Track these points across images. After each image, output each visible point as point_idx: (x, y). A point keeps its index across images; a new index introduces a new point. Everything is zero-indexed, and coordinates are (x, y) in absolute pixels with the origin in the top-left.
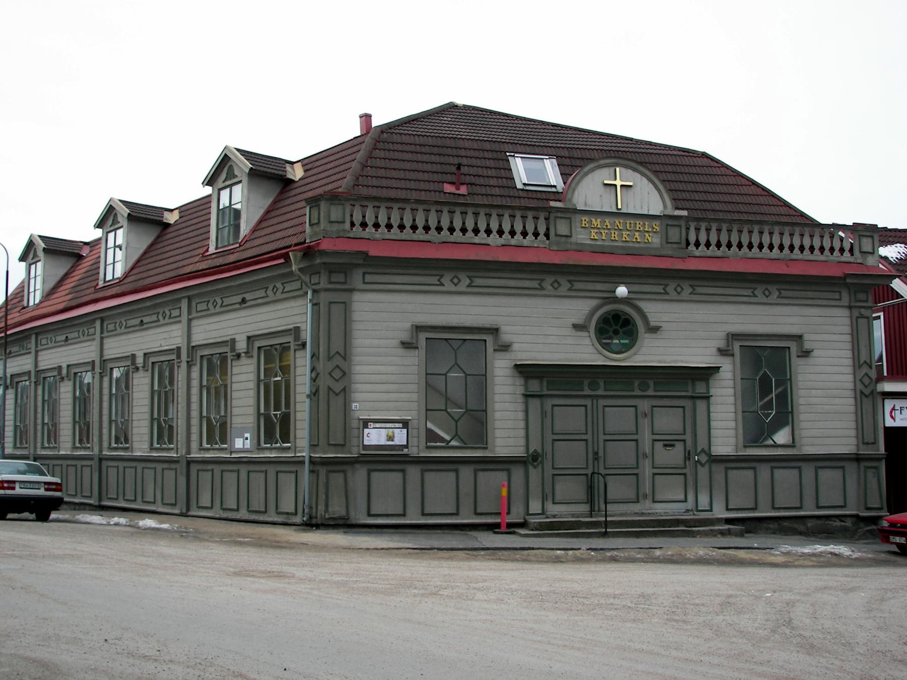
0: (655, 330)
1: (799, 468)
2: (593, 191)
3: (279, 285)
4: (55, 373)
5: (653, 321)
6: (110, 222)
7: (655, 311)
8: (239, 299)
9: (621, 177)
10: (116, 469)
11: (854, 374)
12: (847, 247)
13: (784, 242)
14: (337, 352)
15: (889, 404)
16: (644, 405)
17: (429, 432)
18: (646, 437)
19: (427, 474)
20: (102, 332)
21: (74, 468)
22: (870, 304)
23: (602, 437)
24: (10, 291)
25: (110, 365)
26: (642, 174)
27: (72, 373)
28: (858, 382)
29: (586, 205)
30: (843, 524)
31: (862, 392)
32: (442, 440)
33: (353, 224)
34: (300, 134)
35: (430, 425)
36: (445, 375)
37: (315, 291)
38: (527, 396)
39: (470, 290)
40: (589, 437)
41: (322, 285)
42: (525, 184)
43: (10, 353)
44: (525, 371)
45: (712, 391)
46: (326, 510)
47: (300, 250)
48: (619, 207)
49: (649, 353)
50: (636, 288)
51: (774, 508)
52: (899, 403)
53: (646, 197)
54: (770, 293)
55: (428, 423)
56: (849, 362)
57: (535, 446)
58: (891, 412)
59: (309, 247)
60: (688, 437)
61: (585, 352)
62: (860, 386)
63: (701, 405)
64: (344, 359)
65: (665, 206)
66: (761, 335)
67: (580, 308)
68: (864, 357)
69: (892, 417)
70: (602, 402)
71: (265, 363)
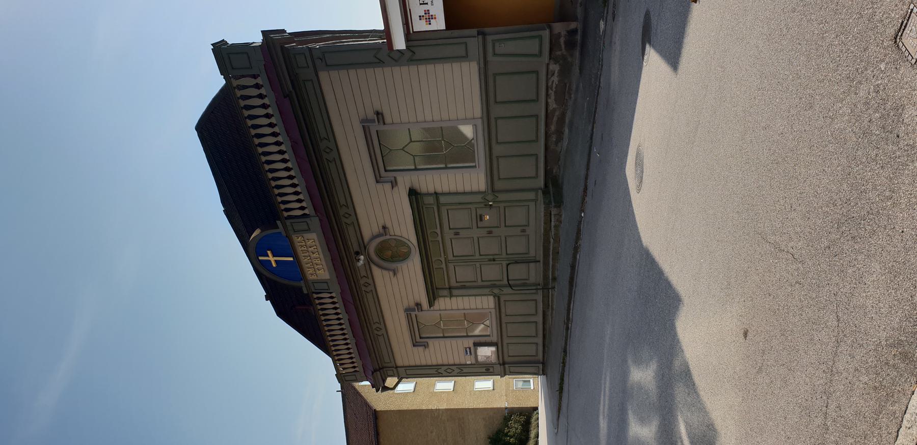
0: (384, 228)
34: (263, 293)
39: (370, 276)
45: (431, 190)
49: (404, 227)
51: (537, 140)
52: (416, 10)
56: (378, 71)
61: (413, 267)
63: (443, 199)
70: (450, 257)
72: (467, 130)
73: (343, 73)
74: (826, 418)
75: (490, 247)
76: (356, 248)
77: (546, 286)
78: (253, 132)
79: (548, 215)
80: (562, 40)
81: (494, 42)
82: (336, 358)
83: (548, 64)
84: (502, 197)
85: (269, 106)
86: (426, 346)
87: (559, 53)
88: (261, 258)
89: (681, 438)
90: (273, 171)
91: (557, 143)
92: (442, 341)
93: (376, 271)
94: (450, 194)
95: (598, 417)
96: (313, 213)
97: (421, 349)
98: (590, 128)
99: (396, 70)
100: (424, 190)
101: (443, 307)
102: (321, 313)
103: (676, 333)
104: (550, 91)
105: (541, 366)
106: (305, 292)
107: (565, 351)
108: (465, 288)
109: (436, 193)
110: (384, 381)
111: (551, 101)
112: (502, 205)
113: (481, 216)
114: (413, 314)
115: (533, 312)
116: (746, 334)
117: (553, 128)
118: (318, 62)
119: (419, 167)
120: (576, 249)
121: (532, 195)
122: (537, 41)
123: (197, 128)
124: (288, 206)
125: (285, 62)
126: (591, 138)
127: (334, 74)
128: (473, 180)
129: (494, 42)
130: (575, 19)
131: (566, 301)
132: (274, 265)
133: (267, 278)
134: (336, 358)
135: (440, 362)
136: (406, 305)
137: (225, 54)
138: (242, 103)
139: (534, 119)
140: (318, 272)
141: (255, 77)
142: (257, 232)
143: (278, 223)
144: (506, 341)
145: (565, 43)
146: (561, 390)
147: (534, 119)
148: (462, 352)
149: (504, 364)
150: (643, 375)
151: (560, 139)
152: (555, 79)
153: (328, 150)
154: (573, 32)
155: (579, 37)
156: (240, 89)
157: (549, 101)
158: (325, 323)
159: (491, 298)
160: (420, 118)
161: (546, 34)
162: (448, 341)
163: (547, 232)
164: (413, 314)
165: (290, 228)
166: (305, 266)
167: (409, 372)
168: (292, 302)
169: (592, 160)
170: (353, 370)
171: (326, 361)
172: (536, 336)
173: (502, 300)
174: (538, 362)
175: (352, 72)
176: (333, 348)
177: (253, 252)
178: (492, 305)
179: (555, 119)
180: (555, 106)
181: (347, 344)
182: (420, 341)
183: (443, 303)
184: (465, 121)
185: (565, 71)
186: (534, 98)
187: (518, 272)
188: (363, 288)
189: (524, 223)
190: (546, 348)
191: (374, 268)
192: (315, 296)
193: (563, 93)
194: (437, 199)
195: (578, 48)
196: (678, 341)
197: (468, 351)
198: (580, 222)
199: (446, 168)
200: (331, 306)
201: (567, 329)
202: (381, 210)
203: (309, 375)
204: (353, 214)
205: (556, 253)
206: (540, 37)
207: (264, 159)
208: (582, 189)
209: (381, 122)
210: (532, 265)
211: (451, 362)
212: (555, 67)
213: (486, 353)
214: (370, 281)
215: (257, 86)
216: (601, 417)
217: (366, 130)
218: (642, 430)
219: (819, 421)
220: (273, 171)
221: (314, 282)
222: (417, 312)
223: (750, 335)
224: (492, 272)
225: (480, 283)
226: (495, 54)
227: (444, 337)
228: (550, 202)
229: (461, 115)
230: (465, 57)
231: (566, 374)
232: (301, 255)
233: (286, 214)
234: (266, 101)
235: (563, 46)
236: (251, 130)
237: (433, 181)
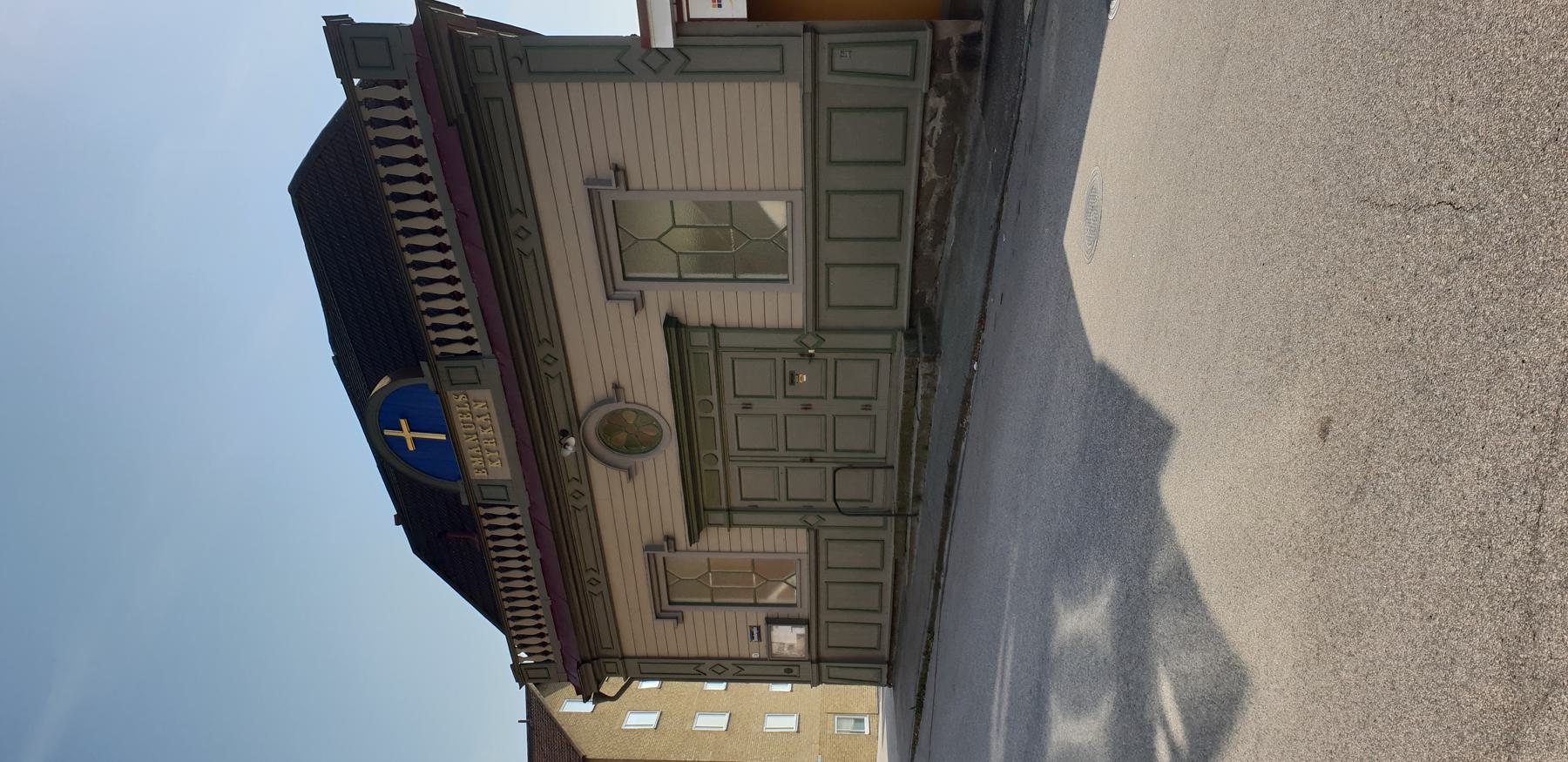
0: (616, 387)
1: (831, 110)
19: (865, 445)
30: (940, 115)
39: (584, 479)
40: (782, 467)
44: (697, 520)
45: (706, 321)
49: (653, 393)
51: (899, 237)
56: (623, 87)
63: (725, 339)
70: (733, 449)
72: (776, 212)
73: (559, 88)
74: (1535, 537)
75: (806, 435)
76: (564, 425)
77: (902, 513)
78: (410, 258)
79: (912, 375)
80: (953, 52)
81: (832, 47)
82: (514, 633)
83: (926, 96)
84: (832, 340)
85: (445, 231)
86: (679, 619)
87: (946, 76)
88: (387, 432)
89: (1161, 709)
90: (442, 342)
91: (934, 245)
92: (709, 612)
93: (596, 468)
94: (739, 329)
95: (988, 729)
96: (488, 351)
97: (670, 624)
98: (996, 203)
99: (655, 88)
100: (692, 320)
101: (714, 547)
102: (491, 544)
103: (1158, 498)
104: (927, 147)
105: (885, 668)
106: (465, 502)
107: (931, 631)
108: (756, 509)
109: (714, 326)
110: (599, 683)
111: (929, 165)
112: (831, 357)
113: (792, 375)
114: (660, 555)
115: (876, 606)
116: (1324, 431)
117: (929, 216)
118: (514, 65)
119: (686, 276)
120: (960, 433)
121: (883, 341)
122: (909, 49)
123: (291, 190)
124: (425, 273)
125: (454, 57)
126: (998, 221)
127: (542, 88)
128: (780, 305)
129: (832, 47)
130: (977, 15)
131: (937, 535)
132: (411, 447)
133: (397, 472)
134: (514, 633)
135: (703, 653)
136: (647, 539)
137: (344, 38)
138: (389, 189)
139: (900, 116)
140: (490, 465)
141: (398, 85)
142: (385, 381)
143: (424, 366)
144: (824, 617)
145: (958, 57)
146: (920, 706)
147: (900, 116)
148: (744, 634)
149: (819, 660)
150: (1084, 620)
151: (940, 238)
152: (938, 124)
153: (550, 360)
154: (973, 39)
155: (983, 48)
156: (391, 183)
157: (925, 165)
158: (497, 565)
159: (802, 533)
160: (693, 182)
161: (925, 38)
162: (719, 612)
163: (909, 406)
164: (660, 555)
165: (444, 377)
166: (468, 452)
167: (645, 668)
168: (443, 526)
169: (998, 251)
170: (544, 658)
171: (494, 641)
172: (879, 611)
173: (824, 534)
174: (879, 661)
175: (575, 88)
176: (509, 615)
177: (376, 420)
178: (803, 547)
179: (934, 200)
180: (934, 175)
181: (535, 608)
182: (667, 609)
183: (717, 538)
184: (774, 193)
185: (956, 112)
186: (899, 157)
187: (853, 486)
188: (572, 502)
189: (869, 392)
190: (892, 634)
191: (595, 465)
192: (483, 511)
193: (949, 153)
194: (716, 338)
195: (982, 67)
196: (1163, 513)
197: (756, 633)
198: (970, 382)
199: (735, 280)
200: (509, 533)
201: (937, 586)
202: (612, 351)
203: (462, 659)
204: (588, 494)
206: (916, 43)
207: (419, 290)
208: (976, 317)
209: (623, 186)
210: (879, 473)
211: (723, 653)
212: (938, 103)
213: (788, 639)
214: (584, 488)
215: (402, 103)
216: (993, 734)
217: (651, 561)
218: (1078, 729)
219: (1518, 550)
220: (438, 327)
221: (482, 484)
222: (666, 553)
223: (1335, 428)
224: (808, 484)
225: (783, 503)
226: (832, 70)
227: (713, 604)
228: (917, 352)
229: (767, 183)
230: (779, 73)
231: (932, 665)
232: (461, 430)
233: (438, 350)
234: (416, 132)
235: (954, 60)
236: (406, 254)
237: (707, 304)
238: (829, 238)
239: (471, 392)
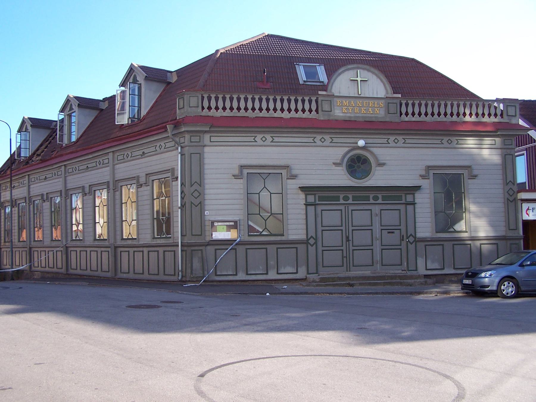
0: (383, 165)
2: (343, 84)
3: (162, 144)
4: (40, 198)
5: (382, 159)
6: (68, 109)
7: (382, 153)
8: (141, 152)
9: (362, 74)
10: (85, 252)
11: (504, 189)
12: (499, 113)
13: (478, 112)
14: (196, 182)
15: (525, 206)
16: (376, 209)
17: (249, 226)
18: (377, 228)
20: (65, 174)
21: (52, 252)
22: (513, 147)
23: (351, 228)
24: (369, 148)
25: (71, 193)
26: (373, 73)
27: (46, 197)
28: (506, 194)
29: (340, 93)
31: (508, 199)
32: (258, 231)
33: (203, 108)
35: (251, 223)
36: (259, 194)
37: (182, 147)
38: (306, 205)
39: (273, 144)
40: (343, 228)
41: (186, 143)
42: (304, 81)
43: (14, 187)
44: (306, 190)
46: (192, 273)
47: (172, 124)
48: (360, 93)
49: (378, 178)
50: (370, 141)
52: (531, 205)
53: (376, 87)
54: (452, 142)
55: (249, 222)
56: (501, 181)
57: (312, 233)
58: (527, 211)
59: (178, 122)
60: (403, 227)
61: (341, 178)
62: (507, 196)
63: (410, 208)
64: (200, 186)
65: (387, 93)
66: (282, 166)
67: (338, 152)
68: (510, 178)
69: (527, 214)
70: (351, 208)
71: (165, 188)
84: (412, 247)
97: (236, 172)
159: (302, 236)
205: (375, 284)
238: (216, 250)
239: (384, 109)
